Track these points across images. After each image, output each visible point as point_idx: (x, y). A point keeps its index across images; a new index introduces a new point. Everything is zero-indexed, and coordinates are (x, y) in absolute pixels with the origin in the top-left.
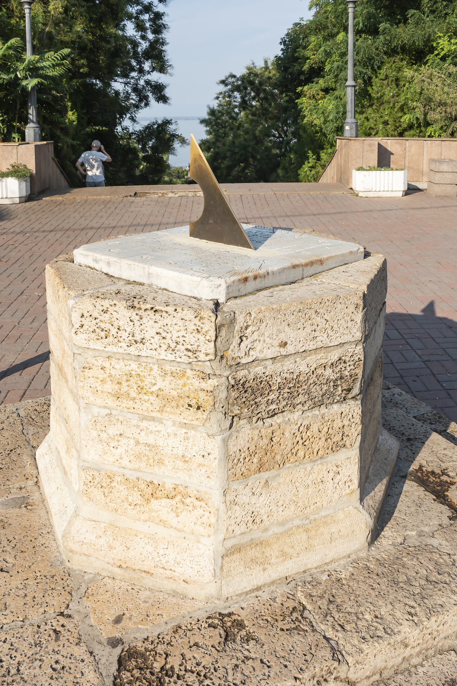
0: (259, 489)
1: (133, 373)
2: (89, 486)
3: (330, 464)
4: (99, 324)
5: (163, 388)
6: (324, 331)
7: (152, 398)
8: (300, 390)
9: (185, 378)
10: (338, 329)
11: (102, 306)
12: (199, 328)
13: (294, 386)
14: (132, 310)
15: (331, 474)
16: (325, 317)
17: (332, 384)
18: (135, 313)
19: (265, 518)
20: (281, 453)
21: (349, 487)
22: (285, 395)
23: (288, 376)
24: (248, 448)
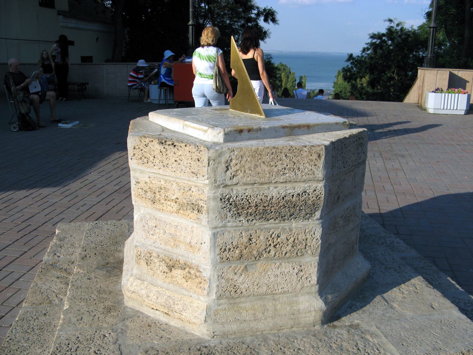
0: (240, 271)
1: (162, 186)
2: (139, 258)
3: (294, 264)
4: (143, 154)
5: (178, 197)
6: (292, 170)
7: (173, 204)
8: (273, 209)
9: (191, 192)
10: (304, 170)
11: (145, 142)
12: (199, 158)
13: (268, 205)
14: (162, 145)
15: (296, 270)
16: (293, 160)
17: (298, 208)
18: (163, 147)
19: (244, 291)
20: (256, 250)
21: (310, 281)
22: (261, 211)
23: (263, 198)
24: (232, 243)
